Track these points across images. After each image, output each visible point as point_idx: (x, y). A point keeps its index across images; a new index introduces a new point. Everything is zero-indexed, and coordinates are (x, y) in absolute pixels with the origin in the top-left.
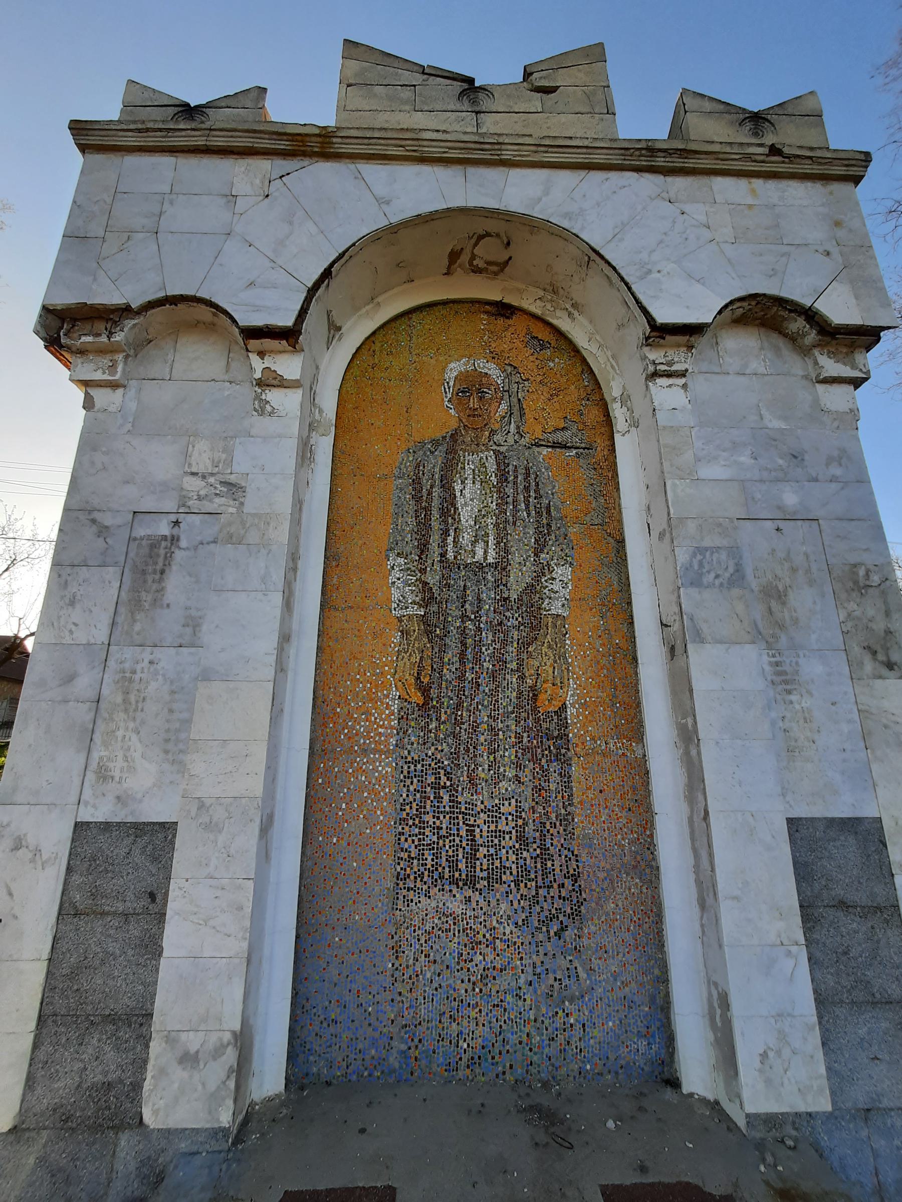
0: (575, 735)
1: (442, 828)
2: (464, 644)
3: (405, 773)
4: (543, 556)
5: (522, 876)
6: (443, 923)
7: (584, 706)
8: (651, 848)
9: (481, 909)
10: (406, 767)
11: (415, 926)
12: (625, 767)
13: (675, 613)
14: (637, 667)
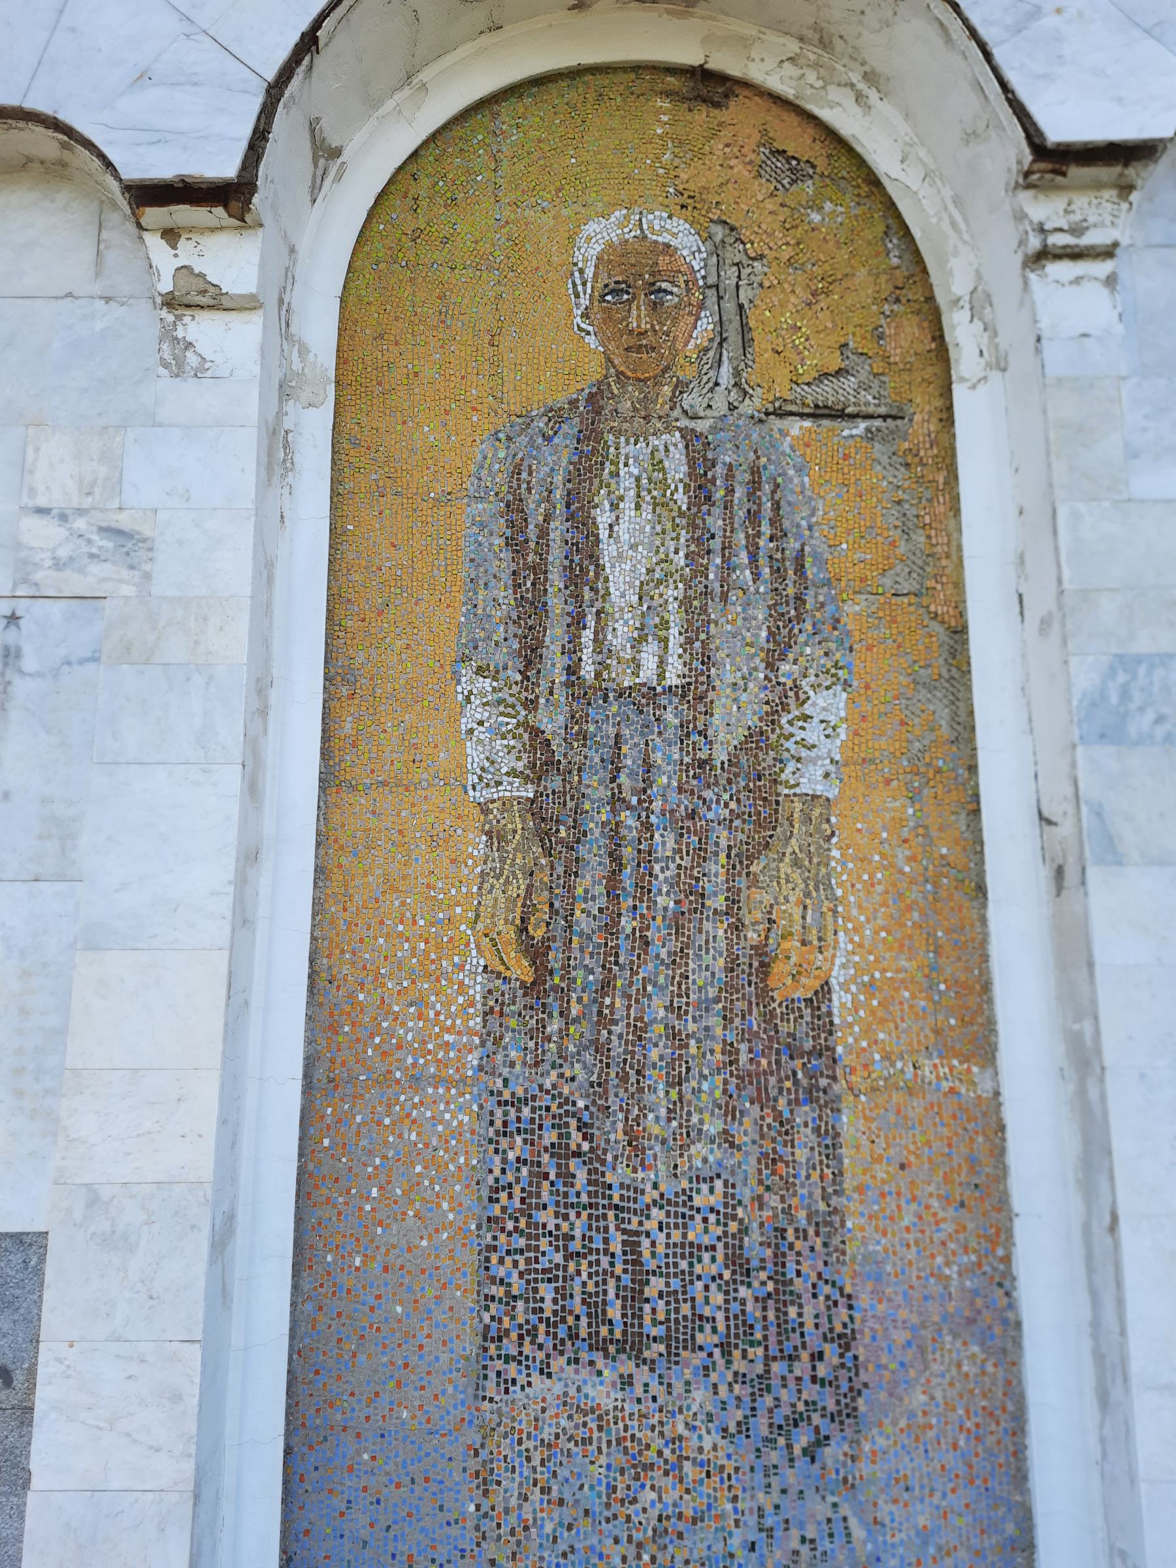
0: (849, 1050)
1: (573, 1238)
2: (615, 857)
3: (498, 1124)
4: (785, 667)
5: (737, 1336)
6: (577, 1427)
7: (870, 988)
8: (1007, 1283)
9: (654, 1399)
10: (499, 1113)
11: (521, 1432)
12: (954, 1117)
13: (1066, 799)
14: (984, 906)
